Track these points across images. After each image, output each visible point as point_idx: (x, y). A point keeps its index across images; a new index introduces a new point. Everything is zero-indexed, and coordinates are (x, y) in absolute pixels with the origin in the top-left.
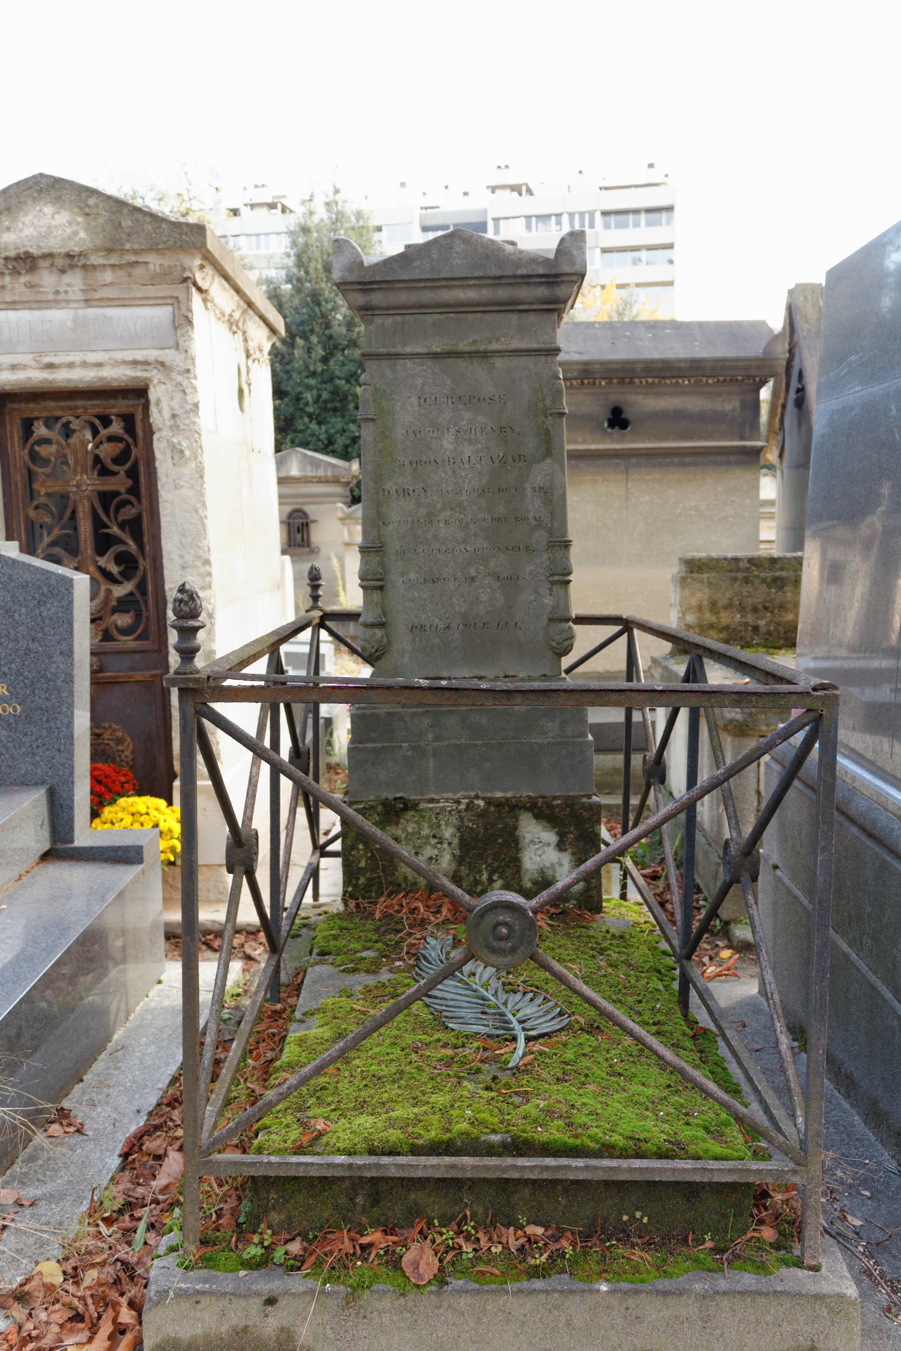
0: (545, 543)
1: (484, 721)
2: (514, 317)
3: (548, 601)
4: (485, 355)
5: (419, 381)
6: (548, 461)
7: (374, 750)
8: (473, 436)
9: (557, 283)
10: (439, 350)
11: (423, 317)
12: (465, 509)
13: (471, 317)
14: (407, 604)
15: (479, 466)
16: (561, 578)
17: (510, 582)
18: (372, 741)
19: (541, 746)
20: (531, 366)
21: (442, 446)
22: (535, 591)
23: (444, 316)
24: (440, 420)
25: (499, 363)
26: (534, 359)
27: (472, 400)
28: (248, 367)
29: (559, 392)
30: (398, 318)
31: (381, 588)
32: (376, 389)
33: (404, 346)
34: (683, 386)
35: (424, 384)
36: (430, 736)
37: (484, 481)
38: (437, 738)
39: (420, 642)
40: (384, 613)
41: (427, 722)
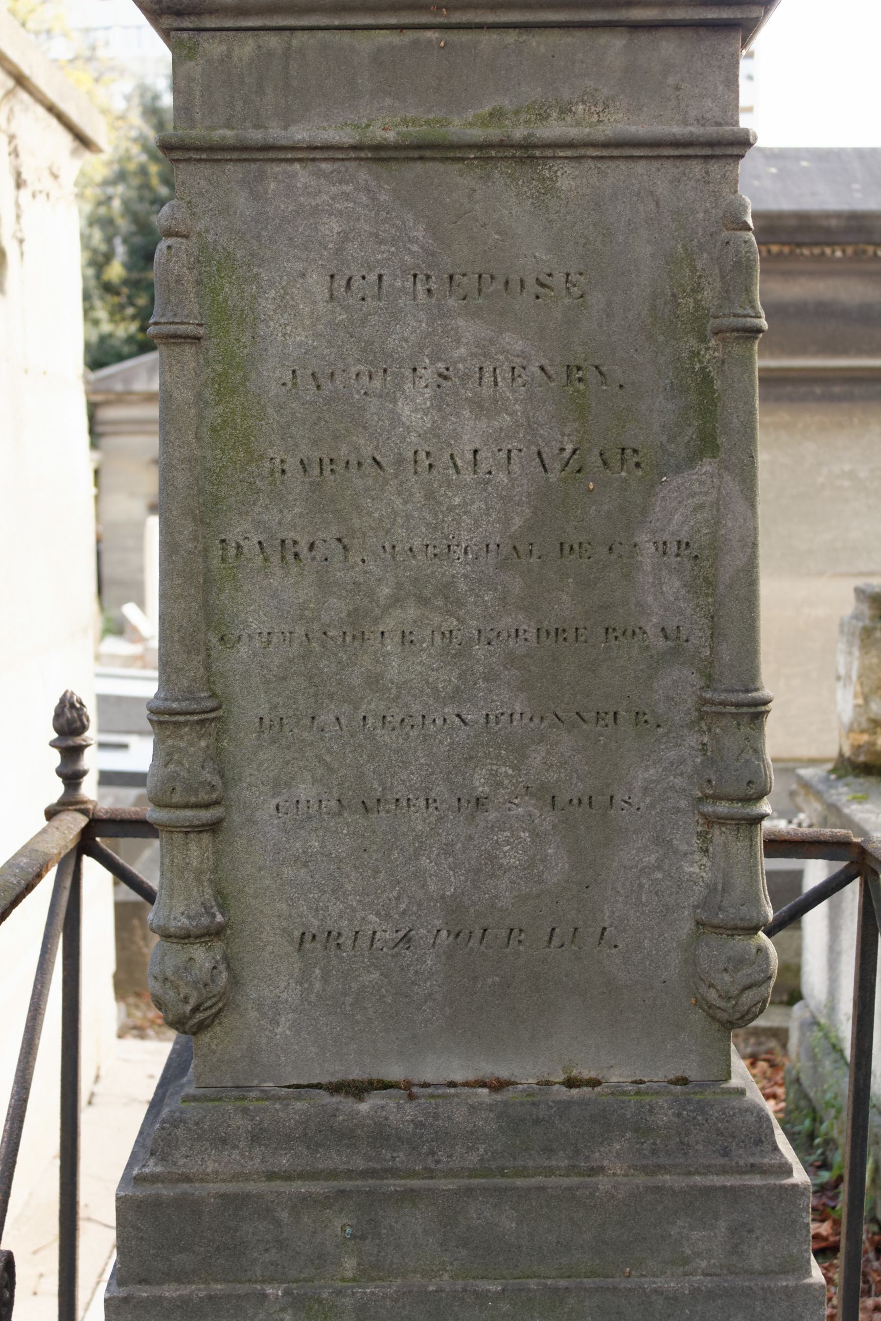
0: (690, 703)
1: (508, 1222)
2: (615, 44)
3: (697, 869)
4: (527, 153)
5: (333, 226)
6: (707, 466)
7: (184, 1303)
8: (486, 391)
9: (533, 157)
10: (391, 136)
11: (345, 38)
12: (460, 603)
13: (488, 39)
14: (288, 872)
15: (502, 477)
16: (738, 809)
17: (587, 813)
18: (181, 1278)
19: (673, 1299)
20: (662, 188)
21: (395, 419)
22: (661, 841)
23: (410, 36)
24: (392, 343)
25: (568, 178)
26: (671, 169)
27: (483, 286)
28: (18, 205)
29: (743, 267)
30: (273, 41)
31: (213, 827)
32: (203, 248)
33: (287, 119)
34: (832, 260)
35: (345, 237)
36: (350, 1265)
37: (518, 521)
38: (369, 1272)
39: (325, 979)
40: (222, 899)
41: (340, 1223)
